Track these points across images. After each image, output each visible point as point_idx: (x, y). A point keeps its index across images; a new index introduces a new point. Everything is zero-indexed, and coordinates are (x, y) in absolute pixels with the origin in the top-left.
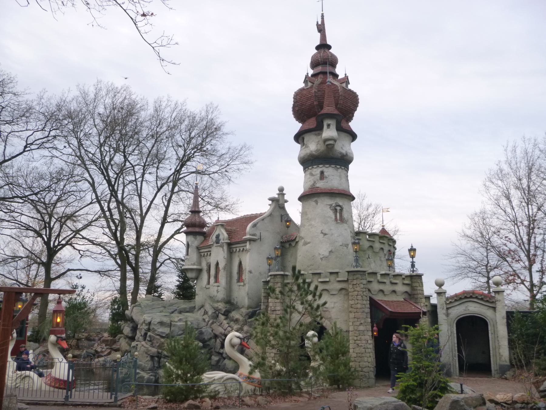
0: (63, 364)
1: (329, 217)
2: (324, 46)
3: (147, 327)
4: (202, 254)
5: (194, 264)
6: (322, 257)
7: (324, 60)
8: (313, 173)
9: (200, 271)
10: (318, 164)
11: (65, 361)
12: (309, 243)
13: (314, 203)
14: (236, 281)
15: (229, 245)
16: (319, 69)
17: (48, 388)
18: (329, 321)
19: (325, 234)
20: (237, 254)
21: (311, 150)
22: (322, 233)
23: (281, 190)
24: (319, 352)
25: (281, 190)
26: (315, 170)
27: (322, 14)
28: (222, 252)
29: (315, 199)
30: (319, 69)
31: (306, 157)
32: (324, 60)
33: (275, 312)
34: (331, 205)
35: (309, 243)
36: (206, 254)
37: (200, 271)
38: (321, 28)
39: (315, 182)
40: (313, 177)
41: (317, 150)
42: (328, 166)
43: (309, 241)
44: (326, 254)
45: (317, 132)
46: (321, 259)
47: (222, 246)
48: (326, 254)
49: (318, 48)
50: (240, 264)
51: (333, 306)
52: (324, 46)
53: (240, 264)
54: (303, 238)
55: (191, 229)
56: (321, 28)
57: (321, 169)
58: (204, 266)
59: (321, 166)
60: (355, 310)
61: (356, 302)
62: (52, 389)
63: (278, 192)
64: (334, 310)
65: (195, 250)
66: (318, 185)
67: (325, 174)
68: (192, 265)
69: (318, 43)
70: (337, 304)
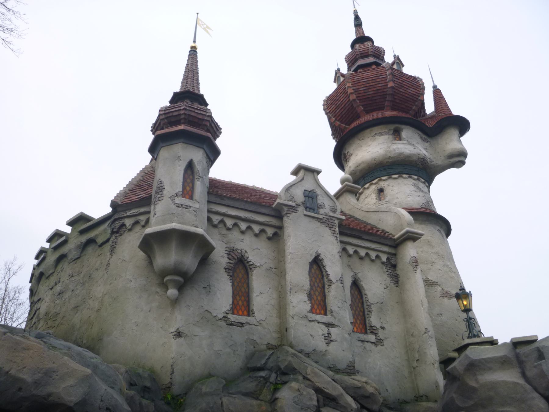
31: (415, 158)
69: (353, 36)
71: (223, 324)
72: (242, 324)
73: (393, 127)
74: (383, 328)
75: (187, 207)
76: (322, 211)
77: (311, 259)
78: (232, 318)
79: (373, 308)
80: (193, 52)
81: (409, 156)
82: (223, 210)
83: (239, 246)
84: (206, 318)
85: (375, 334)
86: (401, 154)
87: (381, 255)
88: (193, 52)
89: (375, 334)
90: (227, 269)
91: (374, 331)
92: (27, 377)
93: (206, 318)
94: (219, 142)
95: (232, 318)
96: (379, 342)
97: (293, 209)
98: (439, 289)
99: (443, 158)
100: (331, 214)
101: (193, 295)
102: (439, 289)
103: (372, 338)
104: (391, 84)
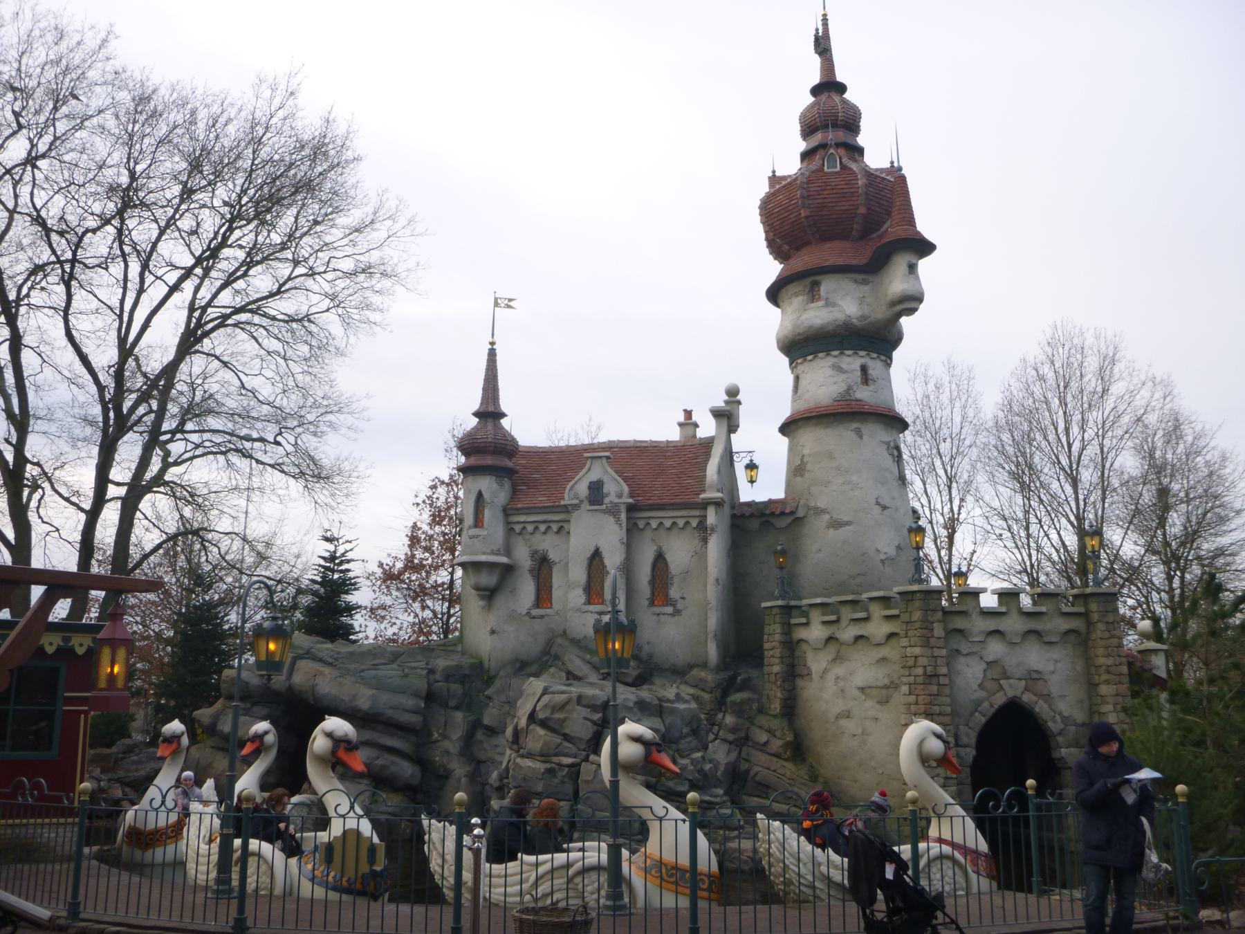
0: (668, 826)
1: (887, 470)
2: (829, 87)
3: (600, 715)
4: (518, 528)
5: (497, 553)
6: (883, 557)
7: (831, 119)
8: (844, 366)
9: (507, 571)
10: (856, 348)
11: (675, 813)
12: (848, 523)
13: (853, 435)
14: (647, 603)
15: (631, 509)
16: (818, 138)
17: (320, 892)
18: (1046, 702)
19: (885, 508)
20: (648, 534)
21: (848, 312)
22: (878, 503)
23: (733, 393)
24: (342, 754)
25: (733, 393)
26: (847, 360)
27: (825, 15)
28: (616, 527)
29: (855, 425)
30: (818, 138)
31: (830, 328)
32: (831, 119)
33: (935, 680)
34: (888, 444)
35: (848, 523)
36: (530, 528)
37: (507, 571)
38: (822, 45)
39: (849, 388)
40: (843, 376)
41: (863, 317)
42: (875, 355)
43: (846, 519)
44: (892, 551)
45: (860, 277)
46: (882, 561)
47: (613, 511)
48: (892, 551)
49: (816, 91)
50: (660, 559)
51: (1052, 668)
52: (829, 87)
53: (660, 559)
54: (820, 512)
55: (474, 461)
56: (822, 45)
57: (862, 361)
58: (522, 555)
59: (862, 353)
60: (1117, 678)
61: (1118, 660)
62: (334, 896)
63: (726, 398)
64: (1055, 678)
65: (501, 515)
66: (858, 395)
67: (871, 372)
68: (493, 553)
69: (816, 79)
70: (1059, 665)
71: (527, 618)
72: (542, 617)
73: (808, 281)
74: (683, 598)
75: (478, 536)
76: (607, 500)
77: (589, 554)
78: (535, 612)
79: (676, 580)
80: (492, 354)
81: (822, 328)
82: (522, 518)
83: (540, 548)
84: (513, 617)
85: (674, 606)
86: (810, 327)
87: (691, 520)
88: (492, 354)
89: (674, 606)
90: (531, 571)
91: (672, 603)
92: (347, 699)
93: (513, 617)
94: (861, 140)
95: (535, 612)
96: (677, 612)
97: (577, 507)
98: (827, 517)
99: (884, 307)
100: (617, 500)
101: (501, 601)
102: (827, 517)
103: (670, 610)
104: (803, 213)
